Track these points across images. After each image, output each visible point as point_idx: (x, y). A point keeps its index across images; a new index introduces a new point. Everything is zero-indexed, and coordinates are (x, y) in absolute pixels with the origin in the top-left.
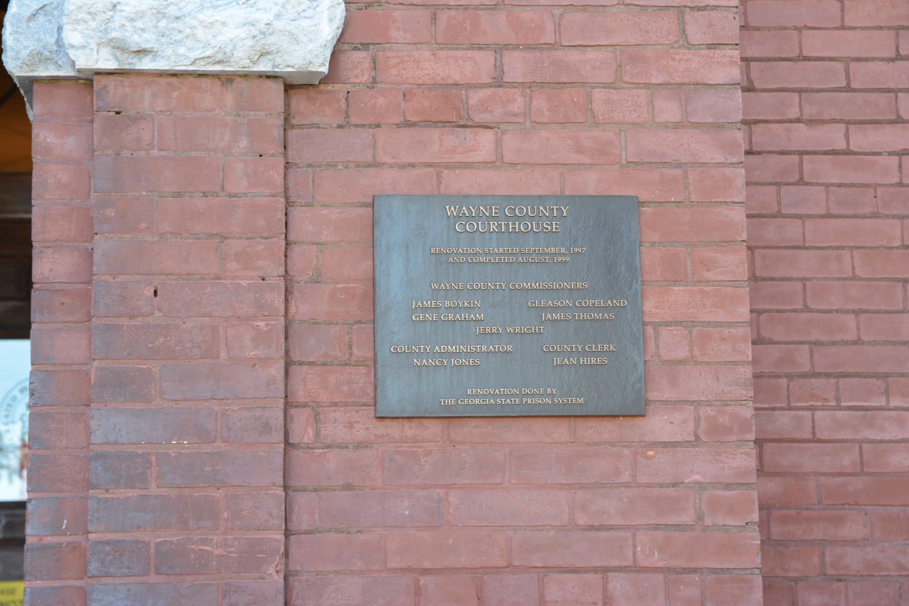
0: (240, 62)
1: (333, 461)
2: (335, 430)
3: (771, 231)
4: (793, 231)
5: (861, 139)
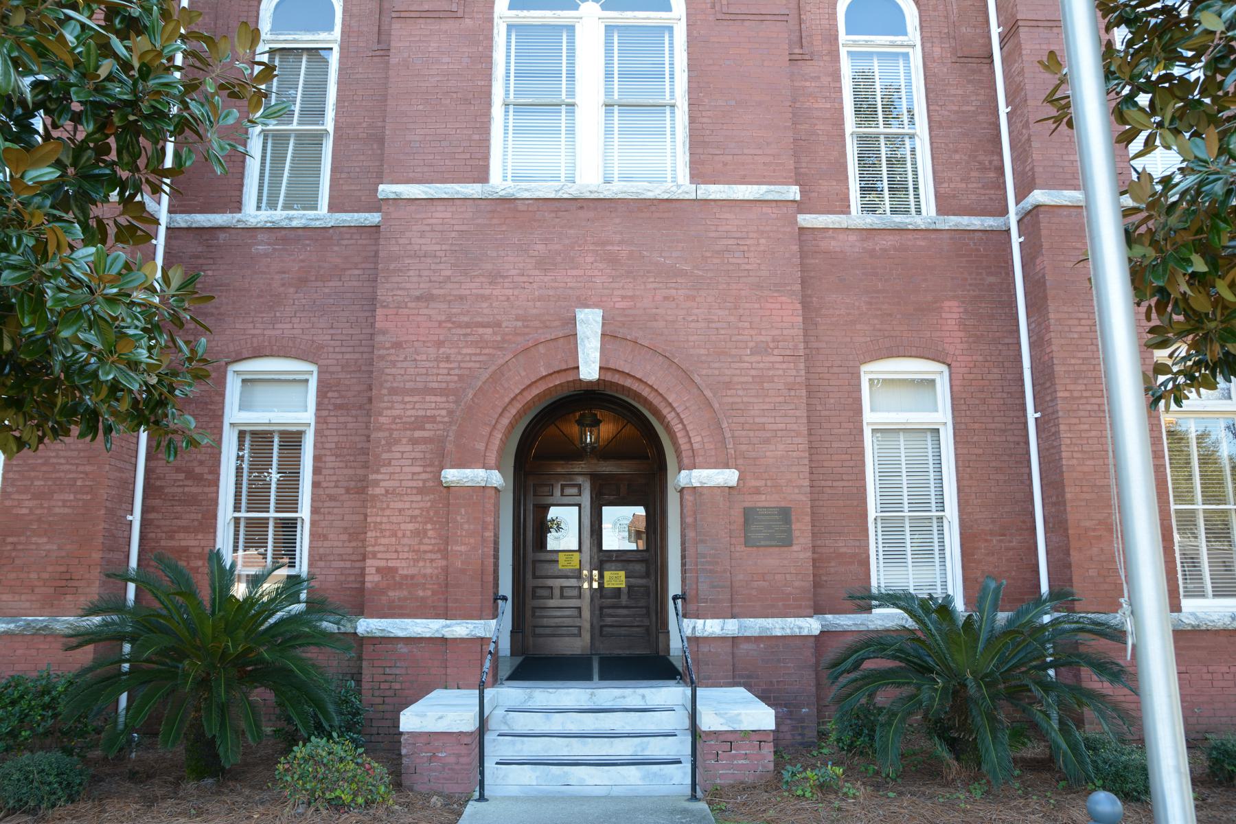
0: (722, 484)
1: (738, 554)
3: (817, 503)
4: (821, 503)
5: (835, 484)
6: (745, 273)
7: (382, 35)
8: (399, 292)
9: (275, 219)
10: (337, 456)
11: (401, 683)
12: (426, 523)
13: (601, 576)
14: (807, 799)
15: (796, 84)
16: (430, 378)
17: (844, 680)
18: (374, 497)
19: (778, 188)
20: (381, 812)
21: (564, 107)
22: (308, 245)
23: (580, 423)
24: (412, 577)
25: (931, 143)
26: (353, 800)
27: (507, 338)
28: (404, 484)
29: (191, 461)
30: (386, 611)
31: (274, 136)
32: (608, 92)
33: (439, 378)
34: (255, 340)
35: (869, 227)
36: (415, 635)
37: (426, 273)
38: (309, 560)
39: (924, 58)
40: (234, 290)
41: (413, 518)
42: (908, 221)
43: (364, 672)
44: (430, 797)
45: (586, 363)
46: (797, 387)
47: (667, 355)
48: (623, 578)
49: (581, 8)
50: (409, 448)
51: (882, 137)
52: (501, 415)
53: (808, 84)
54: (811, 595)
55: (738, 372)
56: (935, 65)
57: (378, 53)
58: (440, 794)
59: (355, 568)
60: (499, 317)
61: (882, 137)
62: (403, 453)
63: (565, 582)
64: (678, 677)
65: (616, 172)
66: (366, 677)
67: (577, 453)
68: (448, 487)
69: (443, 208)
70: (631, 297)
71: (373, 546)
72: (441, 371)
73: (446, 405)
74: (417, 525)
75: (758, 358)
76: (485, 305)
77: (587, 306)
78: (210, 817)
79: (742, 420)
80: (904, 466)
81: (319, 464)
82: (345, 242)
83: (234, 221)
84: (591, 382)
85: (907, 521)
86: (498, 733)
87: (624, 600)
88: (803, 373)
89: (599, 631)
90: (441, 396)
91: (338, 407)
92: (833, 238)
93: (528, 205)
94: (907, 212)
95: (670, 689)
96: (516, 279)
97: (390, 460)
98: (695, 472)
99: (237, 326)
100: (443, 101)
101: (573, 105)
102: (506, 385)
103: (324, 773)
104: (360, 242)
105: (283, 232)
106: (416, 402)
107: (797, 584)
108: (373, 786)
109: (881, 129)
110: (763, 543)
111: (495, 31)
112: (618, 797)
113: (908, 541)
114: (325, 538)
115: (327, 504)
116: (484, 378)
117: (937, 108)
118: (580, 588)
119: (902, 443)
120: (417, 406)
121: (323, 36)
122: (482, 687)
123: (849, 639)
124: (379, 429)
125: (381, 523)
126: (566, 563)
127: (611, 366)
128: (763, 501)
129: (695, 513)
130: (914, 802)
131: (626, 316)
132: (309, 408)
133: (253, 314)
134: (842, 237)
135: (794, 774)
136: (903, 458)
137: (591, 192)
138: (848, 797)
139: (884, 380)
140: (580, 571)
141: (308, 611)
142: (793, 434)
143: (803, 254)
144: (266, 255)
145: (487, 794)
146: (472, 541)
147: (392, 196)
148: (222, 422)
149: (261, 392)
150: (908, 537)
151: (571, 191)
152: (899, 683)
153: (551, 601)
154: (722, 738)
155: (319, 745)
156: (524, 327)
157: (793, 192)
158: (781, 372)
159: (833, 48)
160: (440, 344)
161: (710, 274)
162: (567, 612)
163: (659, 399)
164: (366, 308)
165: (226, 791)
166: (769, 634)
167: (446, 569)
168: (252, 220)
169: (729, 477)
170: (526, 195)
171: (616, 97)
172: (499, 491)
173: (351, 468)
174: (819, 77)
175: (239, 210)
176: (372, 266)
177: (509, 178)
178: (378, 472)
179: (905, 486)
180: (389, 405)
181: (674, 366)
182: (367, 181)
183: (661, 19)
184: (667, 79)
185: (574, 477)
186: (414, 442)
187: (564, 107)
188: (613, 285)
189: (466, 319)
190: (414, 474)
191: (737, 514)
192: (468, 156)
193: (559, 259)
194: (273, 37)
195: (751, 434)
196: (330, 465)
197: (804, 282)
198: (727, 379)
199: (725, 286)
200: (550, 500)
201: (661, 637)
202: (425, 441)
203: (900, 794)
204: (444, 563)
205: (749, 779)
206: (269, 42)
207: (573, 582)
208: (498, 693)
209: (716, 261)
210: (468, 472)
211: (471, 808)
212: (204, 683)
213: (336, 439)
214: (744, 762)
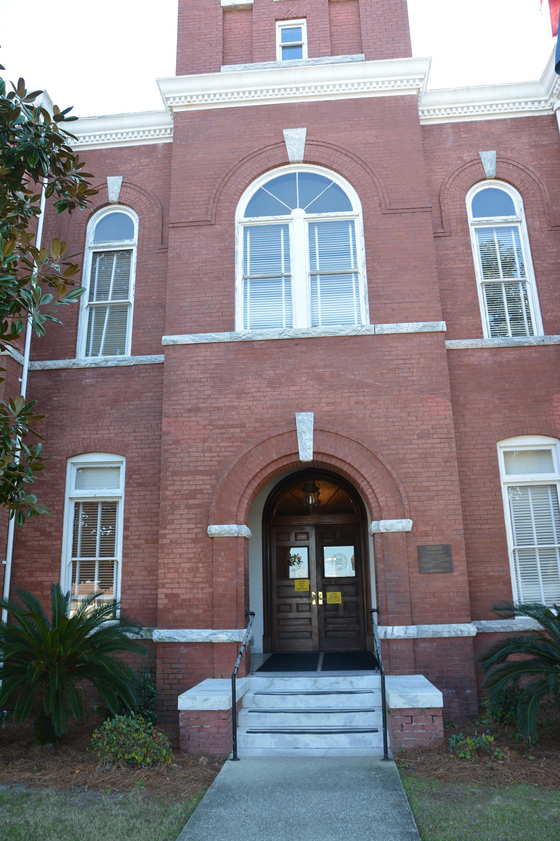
0: (401, 530)
2: (414, 575)
3: (470, 541)
4: (474, 541)
5: (483, 527)
6: (411, 383)
7: (163, 239)
8: (177, 407)
9: (97, 361)
10: (139, 518)
11: (183, 674)
12: (198, 563)
13: (325, 596)
14: (468, 760)
15: (441, 253)
16: (199, 464)
17: (493, 669)
18: (163, 546)
19: (431, 323)
20: (163, 769)
21: (283, 278)
22: (118, 378)
23: (304, 490)
24: (190, 600)
25: (537, 286)
26: (144, 760)
27: (250, 434)
28: (183, 536)
29: (44, 524)
30: (172, 624)
31: (96, 308)
32: (313, 266)
33: (205, 463)
34: (85, 442)
35: (497, 346)
36: (192, 641)
37: (195, 393)
38: (122, 589)
39: (528, 229)
40: (72, 409)
41: (190, 559)
42: (524, 340)
43: (158, 667)
44: (199, 757)
45: (304, 449)
46: (451, 460)
47: (359, 441)
48: (340, 597)
49: (292, 213)
50: (186, 511)
51: (503, 284)
52: (247, 487)
53: (449, 252)
54: (468, 608)
55: (409, 451)
56: (536, 233)
57: (161, 251)
58: (206, 755)
59: (152, 594)
60: (244, 421)
61: (503, 284)
62: (182, 515)
63: (300, 601)
64: (376, 668)
65: (320, 319)
66: (159, 670)
67: (305, 511)
68: (212, 538)
69: (204, 350)
70: (333, 403)
71: (163, 579)
72: (206, 459)
73: (210, 482)
74: (192, 564)
75: (423, 441)
76: (234, 413)
77: (304, 411)
78: (47, 772)
79: (414, 484)
80: (532, 512)
81: (128, 524)
82: (143, 375)
83: (71, 364)
84: (307, 463)
85: (537, 552)
86: (248, 710)
87: (341, 612)
88: (455, 450)
89: (324, 634)
90: (206, 475)
91: (140, 485)
92: (472, 355)
93: (261, 344)
94: (525, 335)
95: (370, 677)
96: (255, 394)
97: (173, 520)
98: (382, 522)
99: (74, 433)
100: (203, 280)
101: (289, 276)
102: (250, 467)
103: (124, 740)
104: (152, 374)
105: (102, 370)
106: (189, 480)
107: (458, 599)
108: (158, 749)
109: (502, 279)
110: (432, 571)
111: (236, 231)
112: (332, 758)
113: (539, 566)
114: (132, 574)
115: (132, 551)
116: (234, 463)
117: (540, 262)
118: (310, 604)
119: (530, 495)
120: (190, 483)
121: (127, 242)
122: (233, 677)
123: (500, 638)
124: (165, 499)
125: (168, 563)
126: (299, 587)
127: (321, 450)
128: (430, 541)
129: (383, 551)
130: (548, 764)
131: (330, 416)
132: (121, 486)
133: (83, 424)
134: (478, 354)
135: (457, 741)
136: (531, 507)
137: (303, 333)
138: (498, 759)
139: (520, 452)
140: (310, 592)
141: (121, 625)
142: (450, 493)
143: (451, 368)
144: (92, 385)
145: (239, 754)
146: (229, 574)
147: (171, 343)
148: (64, 497)
149: (89, 476)
150: (538, 563)
151: (290, 333)
152: (533, 672)
153: (291, 614)
154: (405, 713)
155: (121, 721)
156: (261, 426)
157: (442, 326)
158: (439, 450)
159: (465, 227)
160: (204, 440)
161: (386, 385)
162: (302, 622)
163: (355, 472)
164: (157, 418)
165: (61, 752)
166: (439, 636)
167: (212, 594)
168: (82, 363)
169: (405, 525)
170: (260, 338)
171: (318, 269)
172: (248, 539)
173: (149, 526)
174: (456, 247)
175: (74, 356)
176: (160, 390)
177: (249, 327)
178: (165, 528)
179: (534, 526)
180: (172, 482)
181: (365, 449)
182: (156, 333)
183: (345, 216)
184: (352, 255)
185: (305, 527)
186: (189, 507)
187: (283, 278)
188: (321, 396)
189: (222, 423)
190: (189, 529)
191: (413, 550)
192: (220, 314)
193: (283, 380)
194: (95, 245)
195: (420, 494)
196: (135, 524)
197: (453, 387)
198: (402, 457)
199: (397, 393)
200: (288, 544)
201: (368, 638)
202: (197, 506)
203: (539, 757)
204: (210, 590)
205: (426, 744)
206: (93, 248)
207: (305, 600)
208: (249, 681)
209: (390, 376)
210: (226, 527)
211: (228, 765)
212: (44, 676)
213: (138, 507)
214: (421, 731)
